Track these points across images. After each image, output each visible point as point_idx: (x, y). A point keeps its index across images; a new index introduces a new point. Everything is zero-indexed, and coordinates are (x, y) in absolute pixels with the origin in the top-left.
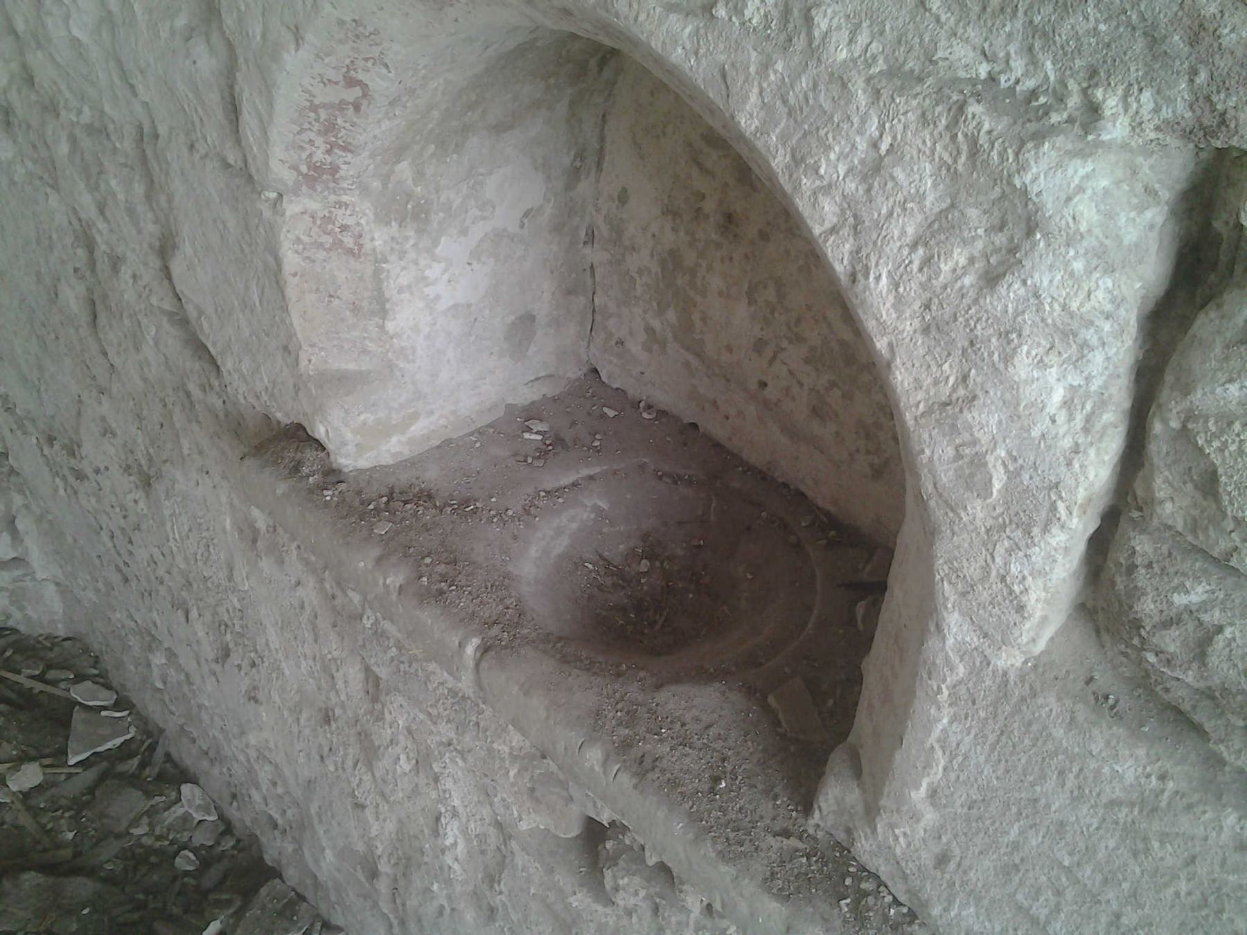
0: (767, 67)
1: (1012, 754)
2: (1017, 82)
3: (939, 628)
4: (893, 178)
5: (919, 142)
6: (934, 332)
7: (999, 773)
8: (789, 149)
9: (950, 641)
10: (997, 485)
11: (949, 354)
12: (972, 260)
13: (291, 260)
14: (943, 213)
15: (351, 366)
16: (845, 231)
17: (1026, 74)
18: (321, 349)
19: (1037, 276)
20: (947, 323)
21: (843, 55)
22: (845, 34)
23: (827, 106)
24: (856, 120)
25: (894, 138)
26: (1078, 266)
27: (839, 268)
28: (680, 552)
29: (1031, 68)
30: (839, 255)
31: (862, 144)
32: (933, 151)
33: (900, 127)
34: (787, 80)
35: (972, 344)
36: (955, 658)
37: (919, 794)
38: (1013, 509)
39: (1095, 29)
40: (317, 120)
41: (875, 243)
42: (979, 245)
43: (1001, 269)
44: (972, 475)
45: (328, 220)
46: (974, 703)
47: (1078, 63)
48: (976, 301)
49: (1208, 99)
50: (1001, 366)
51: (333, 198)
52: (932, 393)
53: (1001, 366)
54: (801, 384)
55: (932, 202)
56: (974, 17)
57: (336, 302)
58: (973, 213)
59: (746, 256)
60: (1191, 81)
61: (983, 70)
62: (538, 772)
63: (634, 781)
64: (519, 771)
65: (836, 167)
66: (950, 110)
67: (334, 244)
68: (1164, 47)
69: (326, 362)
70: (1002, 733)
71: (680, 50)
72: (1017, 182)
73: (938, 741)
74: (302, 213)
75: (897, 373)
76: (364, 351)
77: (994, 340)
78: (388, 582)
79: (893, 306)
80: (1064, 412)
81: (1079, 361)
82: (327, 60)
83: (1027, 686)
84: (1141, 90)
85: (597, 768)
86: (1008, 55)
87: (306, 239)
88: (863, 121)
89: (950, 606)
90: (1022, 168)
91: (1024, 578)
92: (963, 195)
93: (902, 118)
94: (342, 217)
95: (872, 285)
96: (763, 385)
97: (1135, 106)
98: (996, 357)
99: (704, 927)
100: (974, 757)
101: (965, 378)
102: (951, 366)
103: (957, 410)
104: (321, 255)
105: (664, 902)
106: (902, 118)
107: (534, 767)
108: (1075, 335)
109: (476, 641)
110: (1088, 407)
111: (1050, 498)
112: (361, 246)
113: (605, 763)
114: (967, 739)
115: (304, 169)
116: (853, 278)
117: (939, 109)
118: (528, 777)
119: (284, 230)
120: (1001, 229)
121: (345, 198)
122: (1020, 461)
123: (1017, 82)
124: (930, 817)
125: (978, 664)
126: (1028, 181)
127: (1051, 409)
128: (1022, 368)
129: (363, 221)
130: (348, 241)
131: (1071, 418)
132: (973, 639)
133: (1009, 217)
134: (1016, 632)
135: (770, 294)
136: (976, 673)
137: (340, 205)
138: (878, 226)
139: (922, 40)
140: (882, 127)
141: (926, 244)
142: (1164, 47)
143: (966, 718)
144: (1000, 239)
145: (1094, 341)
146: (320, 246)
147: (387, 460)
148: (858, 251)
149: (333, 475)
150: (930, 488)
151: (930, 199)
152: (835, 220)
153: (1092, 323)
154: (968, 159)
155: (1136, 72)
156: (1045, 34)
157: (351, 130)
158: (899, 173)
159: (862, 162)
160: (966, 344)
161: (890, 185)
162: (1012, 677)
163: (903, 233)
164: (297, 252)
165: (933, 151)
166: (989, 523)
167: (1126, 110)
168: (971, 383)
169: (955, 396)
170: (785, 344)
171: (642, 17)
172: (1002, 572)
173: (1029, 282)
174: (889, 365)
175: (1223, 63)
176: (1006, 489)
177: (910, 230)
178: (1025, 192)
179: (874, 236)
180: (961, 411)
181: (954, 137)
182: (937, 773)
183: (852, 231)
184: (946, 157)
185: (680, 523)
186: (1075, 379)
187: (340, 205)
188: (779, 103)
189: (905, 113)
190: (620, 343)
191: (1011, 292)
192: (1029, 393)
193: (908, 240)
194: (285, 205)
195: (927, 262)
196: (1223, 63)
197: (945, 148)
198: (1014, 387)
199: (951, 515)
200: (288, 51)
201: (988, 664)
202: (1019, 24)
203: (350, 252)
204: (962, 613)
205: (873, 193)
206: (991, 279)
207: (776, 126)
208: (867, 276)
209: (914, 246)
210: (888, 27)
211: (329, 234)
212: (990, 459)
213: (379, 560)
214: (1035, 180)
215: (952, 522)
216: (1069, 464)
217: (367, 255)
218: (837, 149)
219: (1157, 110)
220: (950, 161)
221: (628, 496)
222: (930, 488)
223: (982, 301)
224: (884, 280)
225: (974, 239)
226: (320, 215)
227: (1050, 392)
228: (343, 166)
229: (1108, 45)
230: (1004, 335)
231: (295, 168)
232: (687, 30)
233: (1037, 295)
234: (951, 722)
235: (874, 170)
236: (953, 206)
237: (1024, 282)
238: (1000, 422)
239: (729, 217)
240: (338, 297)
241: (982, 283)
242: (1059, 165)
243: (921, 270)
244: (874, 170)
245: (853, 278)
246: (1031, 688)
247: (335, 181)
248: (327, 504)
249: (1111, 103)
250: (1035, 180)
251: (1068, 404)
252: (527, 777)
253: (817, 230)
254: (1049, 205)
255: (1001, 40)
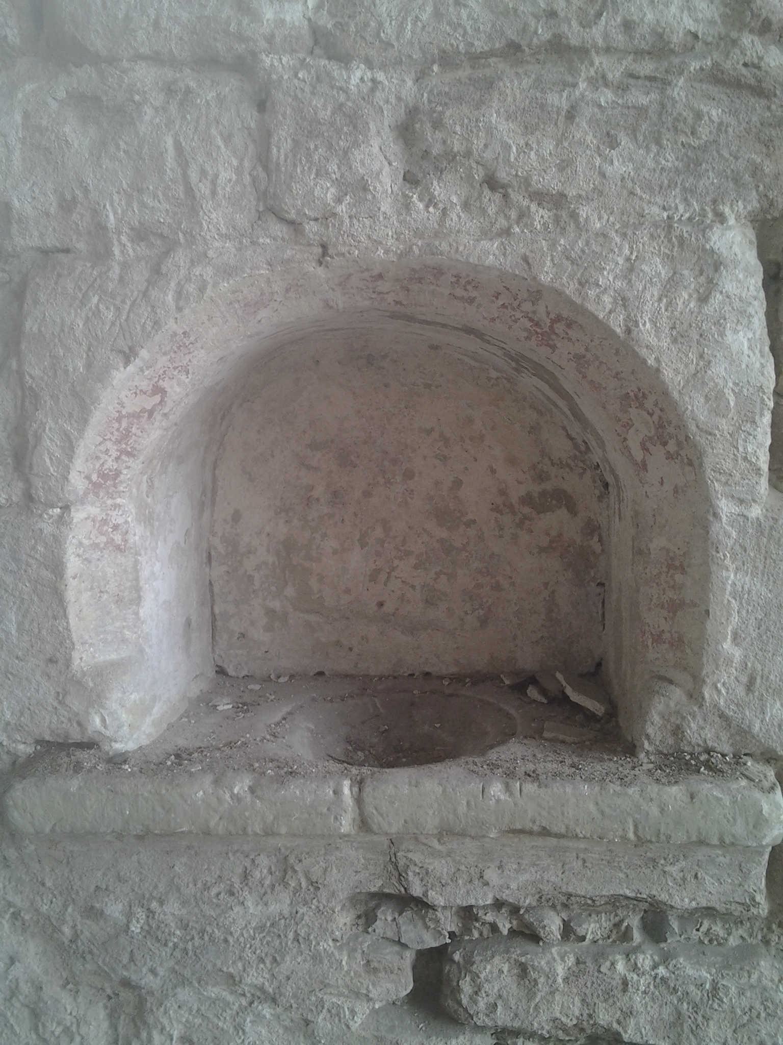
0: (554, 245)
1: (775, 567)
2: (682, 216)
3: (715, 515)
4: (642, 270)
5: (652, 249)
6: (680, 339)
7: (770, 587)
8: (575, 281)
9: (724, 519)
10: (732, 404)
11: (690, 347)
12: (690, 296)
13: (73, 564)
14: (671, 279)
15: (114, 656)
16: (618, 309)
17: (685, 211)
18: (91, 645)
19: (726, 286)
20: (686, 331)
21: (598, 225)
22: (596, 216)
23: (598, 249)
24: (616, 250)
25: (638, 252)
26: (741, 276)
27: (618, 330)
28: (375, 740)
29: (687, 208)
30: (617, 324)
31: (621, 261)
32: (660, 251)
33: (641, 245)
34: (568, 247)
35: (701, 335)
36: (729, 528)
37: (727, 645)
38: (743, 413)
39: (712, 183)
40: (118, 430)
41: (638, 308)
42: (693, 286)
43: (707, 293)
44: (718, 406)
45: (105, 522)
46: (745, 551)
47: (708, 199)
48: (700, 312)
49: (766, 196)
50: (720, 339)
51: (109, 502)
52: (686, 373)
53: (720, 339)
54: (413, 587)
55: (664, 272)
56: (656, 193)
57: (105, 596)
58: (686, 272)
59: (355, 515)
60: (757, 191)
61: (665, 215)
62: (366, 945)
63: (536, 784)
64: (349, 956)
65: (608, 277)
66: (664, 229)
67: (107, 543)
68: (742, 182)
69: (94, 657)
70: (766, 559)
71: (491, 257)
72: (708, 247)
73: (730, 594)
74: (86, 519)
75: (664, 371)
76: (124, 641)
77: (713, 327)
78: (236, 792)
79: (655, 335)
80: (750, 351)
81: (749, 326)
82: (146, 373)
83: (771, 519)
84: (737, 202)
85: (502, 797)
86: (676, 205)
87: (86, 542)
88: (620, 249)
89: (719, 496)
90: (708, 240)
91: (755, 452)
92: (679, 266)
93: (641, 241)
94: (117, 518)
95: (643, 329)
96: (381, 604)
97: (736, 208)
98: (716, 336)
99: (566, 953)
100: (754, 588)
101: (701, 356)
102: (692, 354)
103: (703, 373)
104: (96, 555)
105: (529, 956)
106: (641, 241)
107: (361, 944)
108: (745, 311)
109: (346, 783)
110: (758, 346)
111: (759, 396)
112: (126, 541)
113: (507, 788)
114: (747, 579)
115: (94, 477)
116: (629, 331)
117: (658, 231)
118: (360, 956)
119: (71, 536)
120: (701, 275)
121: (119, 501)
122: (741, 384)
123: (682, 216)
124: (738, 654)
125: (742, 523)
126: (712, 245)
127: (746, 351)
128: (730, 337)
129: (129, 519)
130: (118, 538)
131: (754, 354)
132: (735, 509)
133: (705, 267)
134: (758, 488)
135: (379, 532)
136: (742, 531)
137: (116, 506)
138: (638, 297)
139: (634, 209)
140: (631, 248)
141: (666, 296)
142: (742, 182)
143: (744, 565)
144: (702, 279)
145: (753, 313)
146: (95, 546)
147: (145, 742)
148: (629, 316)
149: (117, 761)
150: (694, 428)
151: (663, 272)
152: (610, 306)
153: (750, 303)
154: (678, 248)
155: (733, 195)
156: (691, 191)
157: (139, 437)
158: (644, 267)
159: (621, 271)
160: (698, 337)
161: (641, 275)
162: (762, 519)
163: (652, 296)
164: (78, 555)
165: (660, 251)
166: (731, 428)
167: (733, 212)
168: (706, 356)
169: (699, 368)
170: (396, 562)
171: (461, 248)
172: (744, 455)
173: (724, 291)
174: (658, 370)
175: (767, 180)
176: (736, 404)
177: (656, 293)
178: (712, 250)
179: (637, 304)
180: (706, 372)
181: (670, 241)
182: (735, 619)
183: (623, 308)
184: (667, 251)
185: (363, 723)
186: (750, 335)
187: (116, 506)
188: (564, 261)
189: (642, 238)
190: (243, 635)
191: (717, 299)
192: (735, 348)
193: (656, 298)
194: (73, 514)
195: (669, 304)
196: (767, 180)
197: (665, 247)
198: (728, 348)
199: (709, 437)
200: (117, 369)
201: (748, 520)
202: (678, 190)
203: (118, 548)
204: (727, 497)
205: (633, 282)
206: (703, 299)
207: (565, 272)
208: (637, 326)
209: (660, 300)
210: (615, 209)
211: (104, 535)
212: (726, 391)
213: (217, 782)
214: (715, 243)
215: (711, 442)
216: (763, 374)
217: (131, 548)
218: (608, 268)
219: (745, 208)
220: (669, 253)
221: (321, 717)
222: (694, 428)
223: (703, 311)
224: (648, 325)
225: (690, 284)
226: (100, 518)
227: (742, 343)
228: (125, 472)
229: (719, 188)
230: (717, 323)
231: (88, 478)
232: (495, 245)
233: (728, 297)
234: (736, 574)
235: (631, 268)
236: (675, 273)
237: (721, 292)
238: (725, 369)
239: (335, 494)
240: (107, 592)
241: (699, 303)
242: (723, 235)
243: (666, 310)
244: (631, 268)
245: (629, 331)
246: (773, 518)
247: (115, 486)
248: (132, 774)
249: (727, 211)
250: (715, 243)
251: (750, 348)
252: (358, 956)
253: (601, 316)
254: (724, 251)
255: (671, 200)
